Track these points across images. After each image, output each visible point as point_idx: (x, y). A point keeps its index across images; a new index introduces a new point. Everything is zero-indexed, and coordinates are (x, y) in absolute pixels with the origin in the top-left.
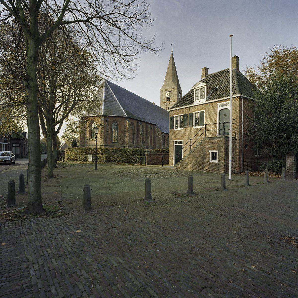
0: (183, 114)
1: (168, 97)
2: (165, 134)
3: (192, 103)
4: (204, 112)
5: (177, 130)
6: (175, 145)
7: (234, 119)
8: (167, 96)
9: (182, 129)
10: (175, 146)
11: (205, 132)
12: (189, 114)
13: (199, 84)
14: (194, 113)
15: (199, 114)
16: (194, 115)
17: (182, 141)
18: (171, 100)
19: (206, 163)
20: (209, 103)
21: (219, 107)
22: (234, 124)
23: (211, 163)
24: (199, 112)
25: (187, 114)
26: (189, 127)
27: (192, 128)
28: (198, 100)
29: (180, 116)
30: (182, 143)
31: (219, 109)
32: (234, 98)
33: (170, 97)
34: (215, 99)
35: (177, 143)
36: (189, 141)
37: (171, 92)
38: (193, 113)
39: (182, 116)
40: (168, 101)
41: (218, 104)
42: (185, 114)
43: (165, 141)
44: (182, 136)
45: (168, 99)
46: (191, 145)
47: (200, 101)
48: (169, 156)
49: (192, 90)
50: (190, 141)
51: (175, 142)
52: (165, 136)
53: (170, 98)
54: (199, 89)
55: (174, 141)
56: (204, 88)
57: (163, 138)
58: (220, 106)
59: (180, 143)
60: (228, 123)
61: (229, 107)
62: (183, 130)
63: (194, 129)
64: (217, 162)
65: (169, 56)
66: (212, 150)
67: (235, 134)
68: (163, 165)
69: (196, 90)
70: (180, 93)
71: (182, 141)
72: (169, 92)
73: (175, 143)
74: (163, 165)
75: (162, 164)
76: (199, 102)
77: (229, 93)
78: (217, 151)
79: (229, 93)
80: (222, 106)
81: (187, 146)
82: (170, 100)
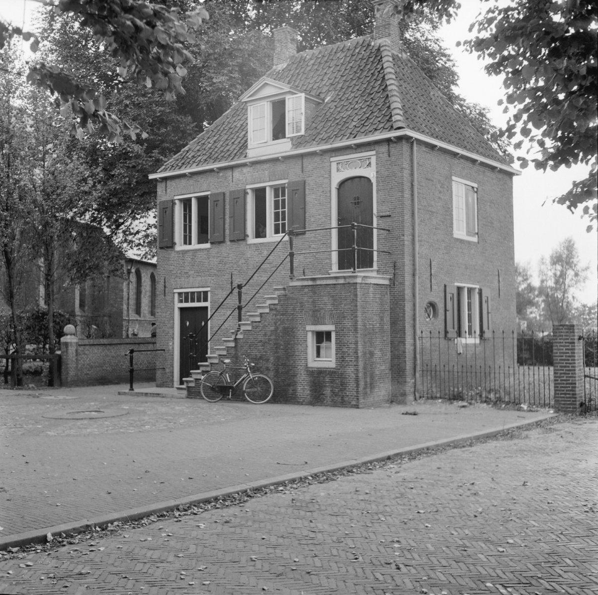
6: (178, 305)
9: (207, 246)
11: (288, 259)
12: (231, 192)
13: (266, 84)
14: (249, 191)
17: (206, 293)
20: (302, 156)
21: (338, 170)
22: (389, 230)
27: (242, 243)
30: (206, 300)
31: (337, 177)
32: (300, 162)
34: (377, 133)
35: (186, 301)
36: (231, 292)
50: (236, 291)
51: (180, 294)
60: (382, 217)
61: (371, 173)
64: (455, 236)
66: (316, 323)
68: (131, 386)
71: (206, 293)
73: (181, 301)
74: (131, 386)
75: (126, 382)
77: (245, 139)
79: (245, 139)
81: (225, 312)
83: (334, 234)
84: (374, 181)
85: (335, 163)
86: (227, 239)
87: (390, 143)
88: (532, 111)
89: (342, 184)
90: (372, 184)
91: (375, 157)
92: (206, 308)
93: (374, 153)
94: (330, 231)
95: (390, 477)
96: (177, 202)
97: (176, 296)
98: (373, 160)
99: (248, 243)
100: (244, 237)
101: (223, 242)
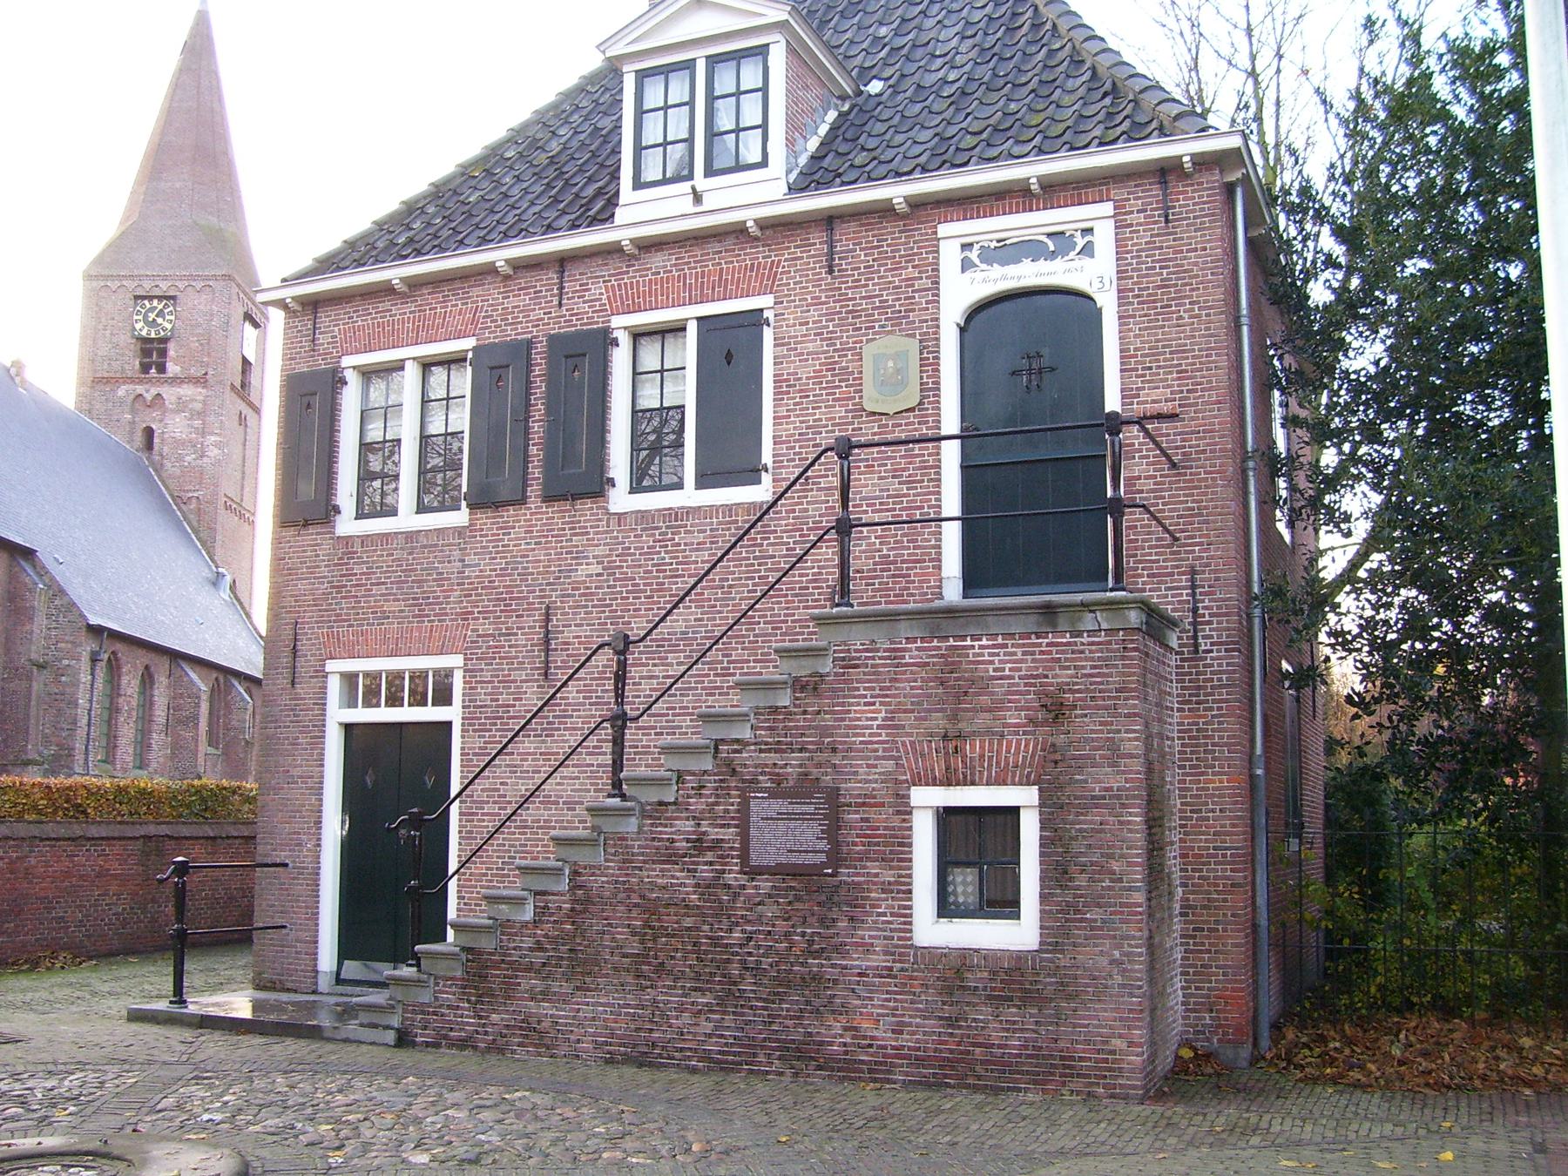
0: (468, 343)
1: (151, 340)
2: (119, 647)
3: (605, 217)
4: (755, 319)
5: (385, 537)
6: (338, 714)
7: (1166, 408)
8: (144, 333)
10: (349, 728)
15: (688, 351)
16: (620, 359)
18: (172, 368)
19: (857, 961)
20: (830, 220)
21: (966, 265)
23: (934, 956)
24: (692, 328)
25: (529, 344)
26: (548, 498)
28: (685, 187)
29: (427, 365)
30: (444, 698)
33: (165, 340)
37: (173, 298)
38: (606, 332)
39: (451, 362)
40: (145, 368)
41: (953, 232)
42: (490, 338)
43: (113, 710)
44: (453, 608)
45: (146, 353)
46: (620, 721)
47: (697, 197)
48: (1041, 806)
49: (613, 70)
51: (350, 679)
52: (114, 667)
53: (163, 353)
54: (690, 65)
55: (332, 666)
56: (762, 51)
57: (99, 684)
58: (974, 255)
59: (419, 700)
62: (459, 531)
63: (621, 516)
65: (181, 32)
66: (949, 781)
67: (1184, 580)
69: (642, 75)
70: (256, 325)
72: (160, 298)
76: (687, 205)
78: (1024, 797)
80: (1005, 252)
82: (162, 369)
83: (952, 535)
84: (1108, 303)
85: (957, 244)
86: (534, 490)
87: (1171, 178)
88: (1397, 568)
89: (977, 311)
90: (1098, 313)
91: (1111, 223)
92: (448, 725)
93: (1107, 208)
94: (939, 448)
95: (956, 1143)
96: (352, 377)
97: (334, 686)
98: (1105, 236)
99: (613, 509)
100: (598, 486)
101: (522, 501)
